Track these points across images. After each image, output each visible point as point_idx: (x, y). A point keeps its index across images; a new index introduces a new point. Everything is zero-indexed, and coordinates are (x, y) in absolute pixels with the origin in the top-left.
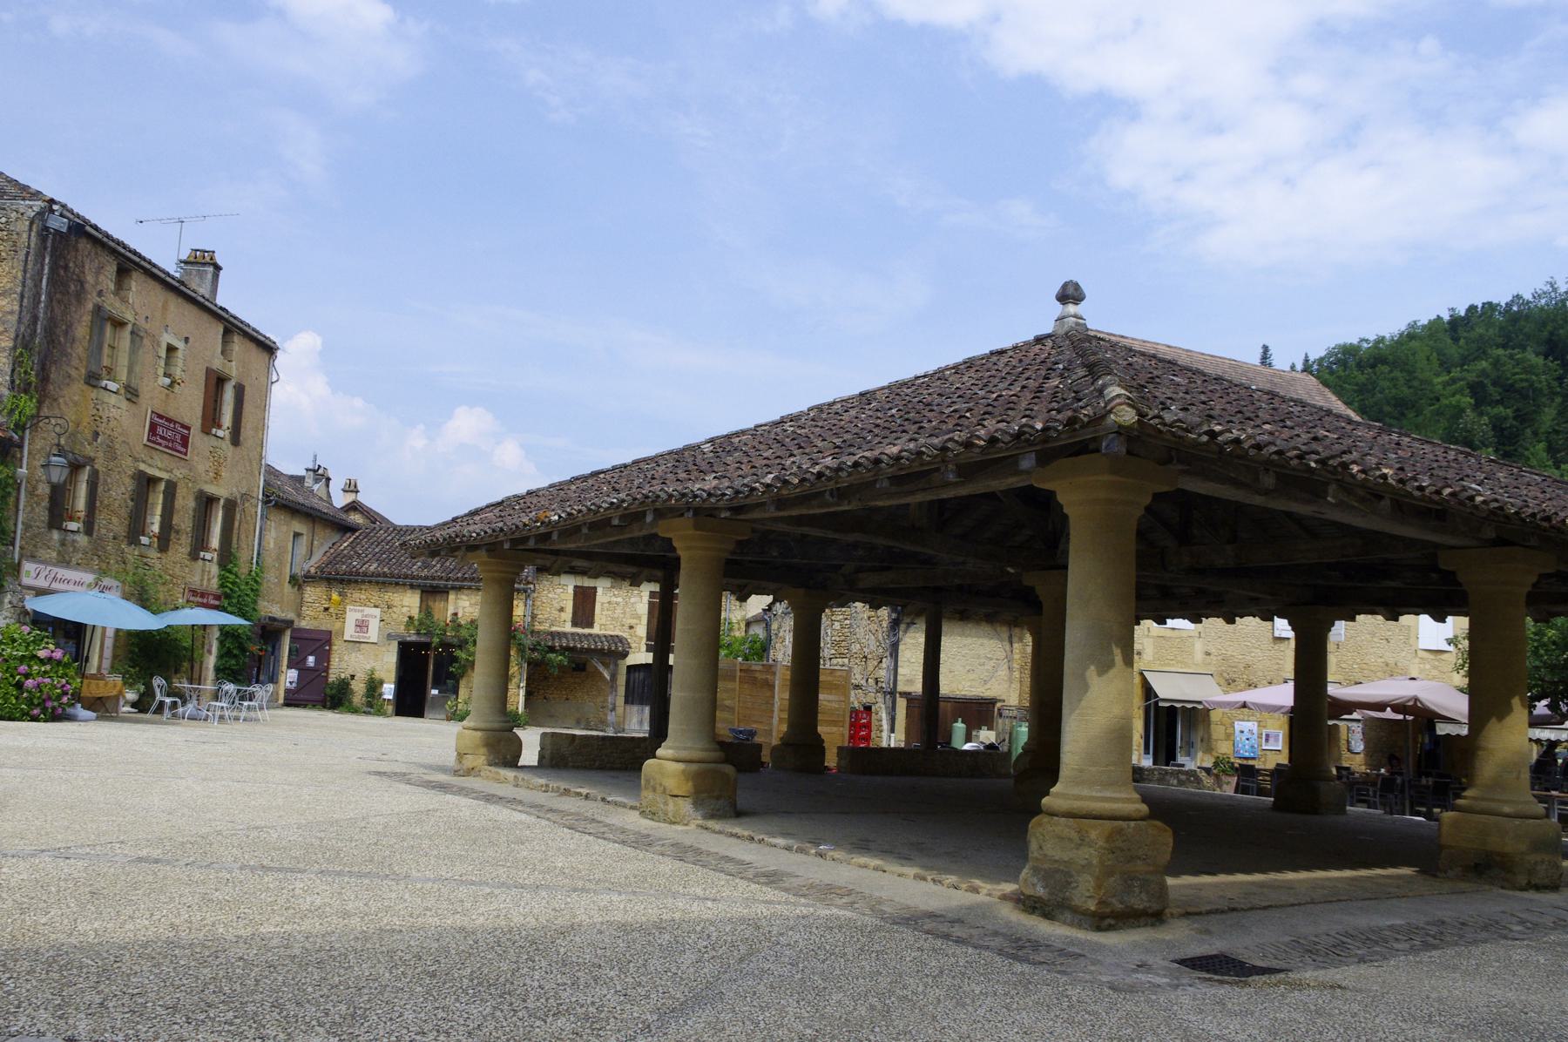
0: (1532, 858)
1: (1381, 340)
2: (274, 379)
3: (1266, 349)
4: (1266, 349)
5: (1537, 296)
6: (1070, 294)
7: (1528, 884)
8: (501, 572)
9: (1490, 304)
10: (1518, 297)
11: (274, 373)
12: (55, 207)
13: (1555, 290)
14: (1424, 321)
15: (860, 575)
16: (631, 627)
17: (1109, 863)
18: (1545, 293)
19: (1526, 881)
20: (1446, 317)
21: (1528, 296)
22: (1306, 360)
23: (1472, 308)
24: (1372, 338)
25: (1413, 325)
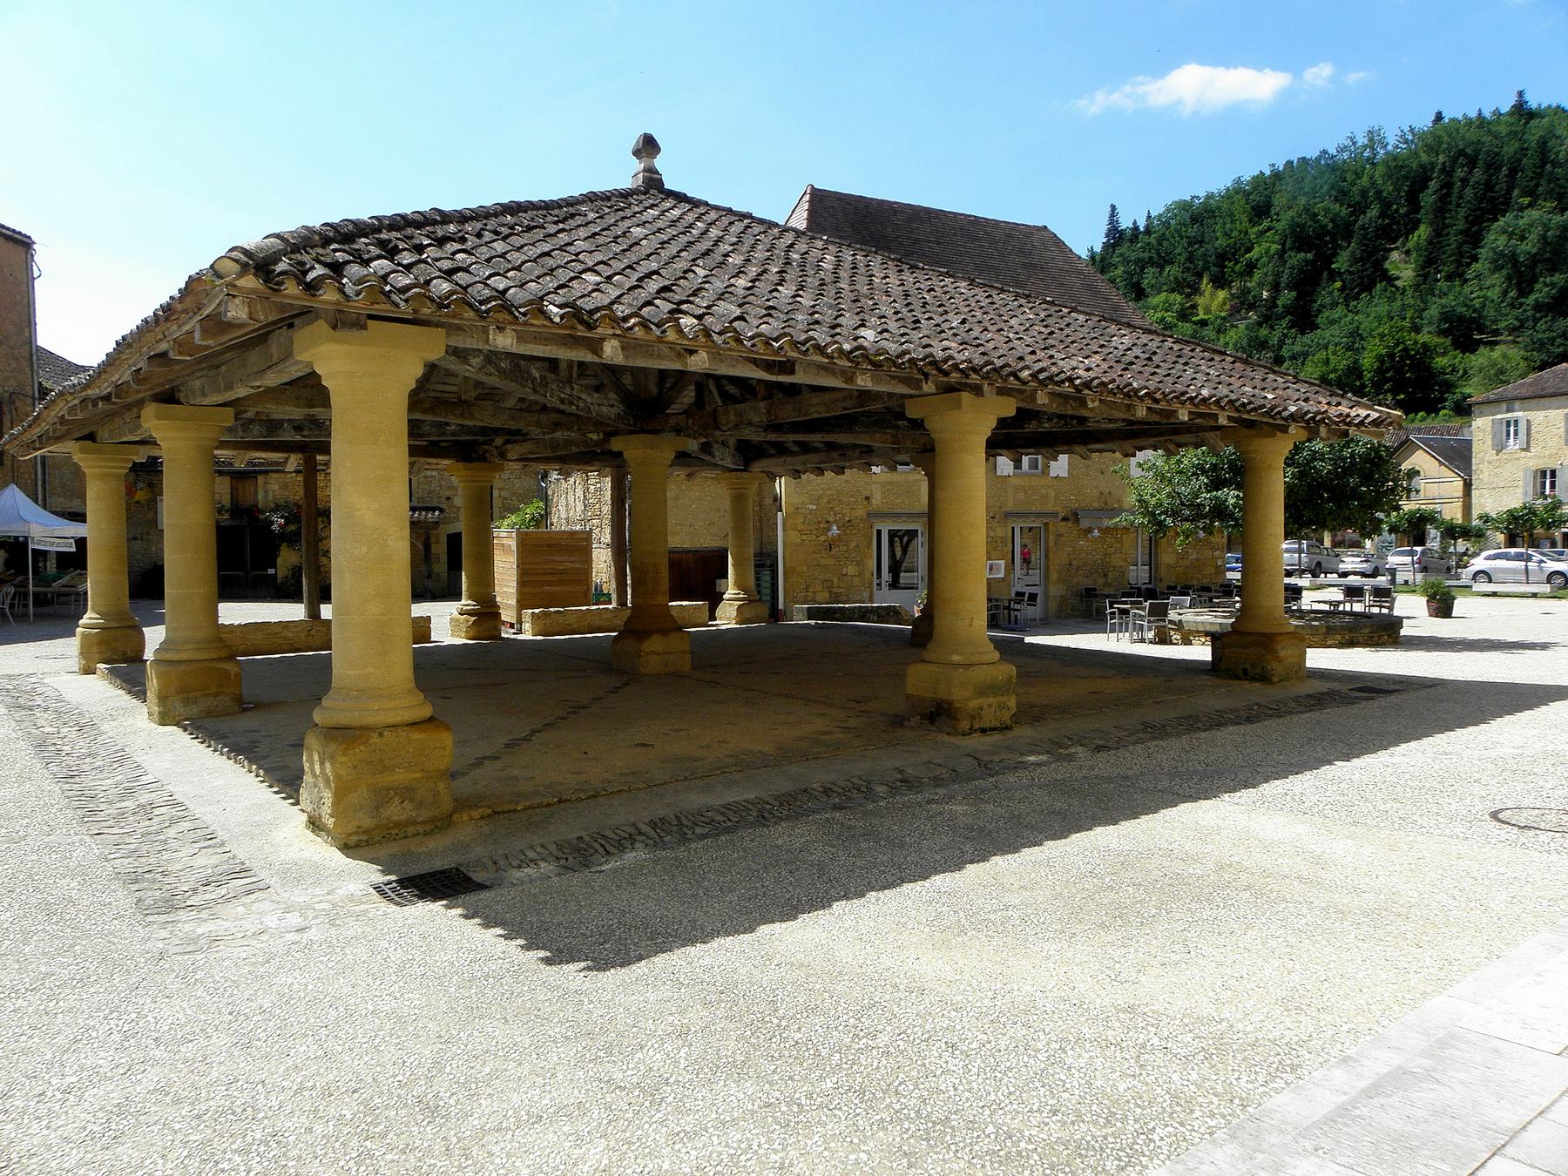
0: (974, 703)
1: (1210, 196)
2: (36, 273)
3: (1113, 208)
4: (1113, 208)
5: (1341, 150)
6: (648, 146)
7: (970, 729)
8: (99, 467)
9: (1304, 158)
10: (1325, 152)
11: (35, 268)
12: (1527, 200)
13: (1354, 144)
14: (1247, 177)
15: (509, 446)
16: (448, 498)
17: (349, 778)
18: (1345, 147)
19: (969, 726)
20: (1268, 173)
21: (1333, 151)
22: (1149, 217)
23: (1290, 163)
24: (1202, 194)
25: (1238, 181)
